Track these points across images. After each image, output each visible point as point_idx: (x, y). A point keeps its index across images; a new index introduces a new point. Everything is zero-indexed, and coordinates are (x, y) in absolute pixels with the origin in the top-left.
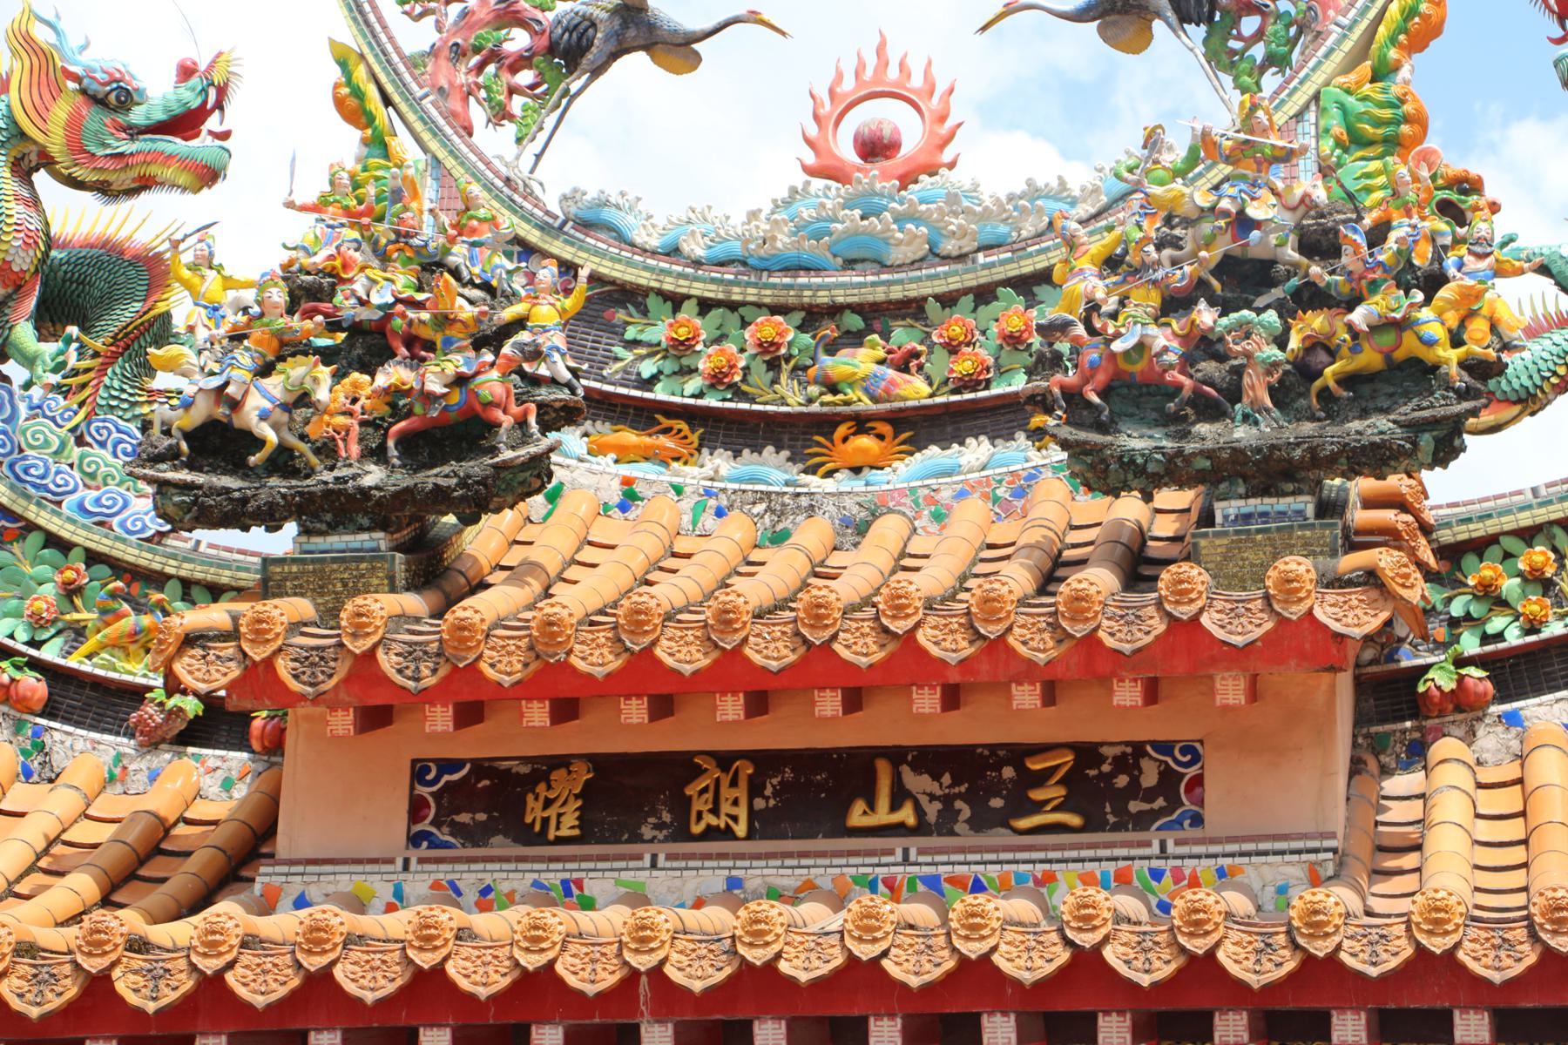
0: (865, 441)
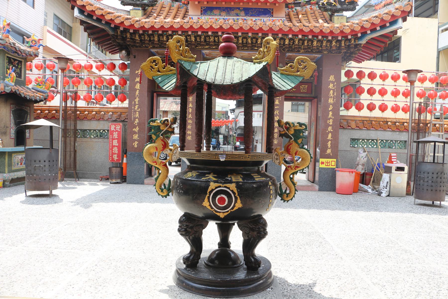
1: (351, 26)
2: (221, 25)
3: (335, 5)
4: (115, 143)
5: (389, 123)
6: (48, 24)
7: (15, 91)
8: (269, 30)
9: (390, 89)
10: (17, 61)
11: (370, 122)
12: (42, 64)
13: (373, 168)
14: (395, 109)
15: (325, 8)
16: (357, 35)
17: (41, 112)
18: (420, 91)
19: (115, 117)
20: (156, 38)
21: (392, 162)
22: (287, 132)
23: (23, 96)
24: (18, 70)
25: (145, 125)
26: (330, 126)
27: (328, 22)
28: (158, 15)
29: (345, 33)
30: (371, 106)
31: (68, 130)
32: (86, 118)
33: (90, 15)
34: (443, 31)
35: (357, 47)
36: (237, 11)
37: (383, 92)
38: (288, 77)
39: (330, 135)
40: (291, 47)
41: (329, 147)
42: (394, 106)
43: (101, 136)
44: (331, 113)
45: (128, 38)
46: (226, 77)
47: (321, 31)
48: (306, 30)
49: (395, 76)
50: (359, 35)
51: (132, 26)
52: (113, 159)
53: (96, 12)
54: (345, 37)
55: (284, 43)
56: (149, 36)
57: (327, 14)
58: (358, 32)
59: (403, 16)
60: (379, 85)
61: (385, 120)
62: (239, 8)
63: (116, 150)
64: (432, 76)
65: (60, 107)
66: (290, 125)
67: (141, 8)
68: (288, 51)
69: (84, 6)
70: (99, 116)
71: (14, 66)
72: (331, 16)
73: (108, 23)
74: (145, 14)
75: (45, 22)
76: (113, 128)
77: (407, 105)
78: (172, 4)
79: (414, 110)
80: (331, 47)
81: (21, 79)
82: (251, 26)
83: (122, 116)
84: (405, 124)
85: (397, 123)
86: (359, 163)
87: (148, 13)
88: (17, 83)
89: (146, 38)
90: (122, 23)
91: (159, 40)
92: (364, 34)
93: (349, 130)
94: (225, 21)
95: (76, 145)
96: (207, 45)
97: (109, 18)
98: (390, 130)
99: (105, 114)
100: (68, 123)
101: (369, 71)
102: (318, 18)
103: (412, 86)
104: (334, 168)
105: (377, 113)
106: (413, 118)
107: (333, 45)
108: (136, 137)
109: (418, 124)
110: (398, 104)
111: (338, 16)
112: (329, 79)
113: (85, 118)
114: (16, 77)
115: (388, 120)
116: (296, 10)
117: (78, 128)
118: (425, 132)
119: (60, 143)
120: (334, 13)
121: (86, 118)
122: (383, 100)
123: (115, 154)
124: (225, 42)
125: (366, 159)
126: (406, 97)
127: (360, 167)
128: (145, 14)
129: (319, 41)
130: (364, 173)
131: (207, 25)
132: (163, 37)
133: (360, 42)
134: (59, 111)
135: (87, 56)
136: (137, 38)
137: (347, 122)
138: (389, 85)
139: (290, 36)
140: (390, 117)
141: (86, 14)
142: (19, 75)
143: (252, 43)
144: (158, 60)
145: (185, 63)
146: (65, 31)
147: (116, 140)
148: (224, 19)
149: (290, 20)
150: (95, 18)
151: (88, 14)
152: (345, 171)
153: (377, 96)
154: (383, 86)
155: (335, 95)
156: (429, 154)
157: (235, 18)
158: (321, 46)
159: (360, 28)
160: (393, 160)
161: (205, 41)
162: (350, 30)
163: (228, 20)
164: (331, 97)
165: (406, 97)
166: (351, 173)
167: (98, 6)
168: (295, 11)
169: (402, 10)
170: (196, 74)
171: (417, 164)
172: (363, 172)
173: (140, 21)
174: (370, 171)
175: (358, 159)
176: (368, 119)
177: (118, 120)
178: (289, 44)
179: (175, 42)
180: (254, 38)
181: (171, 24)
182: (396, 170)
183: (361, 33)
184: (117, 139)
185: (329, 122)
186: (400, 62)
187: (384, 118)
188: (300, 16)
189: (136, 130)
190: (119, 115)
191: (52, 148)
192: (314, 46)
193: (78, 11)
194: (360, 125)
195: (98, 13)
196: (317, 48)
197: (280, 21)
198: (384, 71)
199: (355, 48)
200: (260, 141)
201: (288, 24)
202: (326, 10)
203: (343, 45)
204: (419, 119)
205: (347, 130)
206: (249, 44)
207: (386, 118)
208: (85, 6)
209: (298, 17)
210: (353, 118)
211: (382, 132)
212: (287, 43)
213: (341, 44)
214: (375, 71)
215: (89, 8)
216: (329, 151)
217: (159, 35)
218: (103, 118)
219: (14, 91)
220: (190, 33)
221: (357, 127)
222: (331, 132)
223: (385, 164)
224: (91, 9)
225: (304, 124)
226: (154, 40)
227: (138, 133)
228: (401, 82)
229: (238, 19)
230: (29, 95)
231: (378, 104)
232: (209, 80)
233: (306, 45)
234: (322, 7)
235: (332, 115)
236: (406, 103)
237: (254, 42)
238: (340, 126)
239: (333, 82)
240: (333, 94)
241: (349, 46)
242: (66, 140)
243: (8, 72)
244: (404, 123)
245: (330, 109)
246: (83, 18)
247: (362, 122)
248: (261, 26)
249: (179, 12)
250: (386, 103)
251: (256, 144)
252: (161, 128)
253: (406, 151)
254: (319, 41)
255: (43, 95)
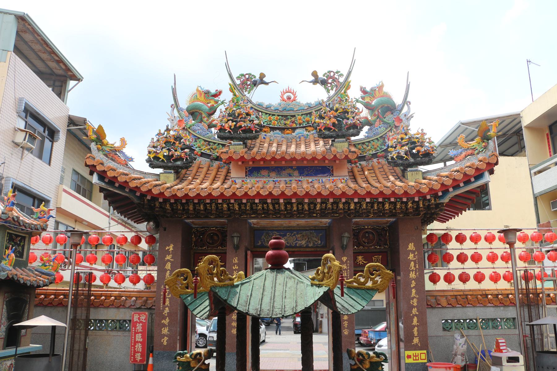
0: (288, 131)
1: (429, 183)
2: (270, 190)
3: (406, 158)
4: (139, 338)
5: (489, 296)
6: (65, 181)
7: (13, 277)
8: (329, 194)
9: (485, 254)
10: (19, 237)
11: (464, 297)
12: (51, 238)
13: (476, 358)
14: (495, 278)
15: (395, 162)
16: (437, 194)
17: (45, 297)
18: (523, 253)
19: (139, 303)
20: (191, 207)
21: (501, 351)
22: (361, 367)
23: (22, 282)
24: (20, 248)
25: (177, 316)
26: (414, 307)
27: (401, 178)
28: (194, 178)
29: (423, 193)
30: (464, 277)
31: (78, 320)
32: (103, 305)
33: (112, 181)
34: (535, 174)
35: (439, 207)
36: (289, 171)
37: (476, 258)
38: (357, 291)
39: (415, 320)
40: (358, 212)
41: (416, 335)
42: (493, 274)
43: (120, 328)
44: (414, 291)
45: (157, 208)
46: (275, 305)
47: (393, 192)
48: (375, 192)
49: (490, 236)
50: (440, 194)
51: (162, 194)
52: (135, 360)
53: (119, 179)
54: (423, 197)
55: (349, 208)
56: (182, 204)
57: (398, 170)
58: (439, 190)
59: (489, 168)
60: (471, 249)
61: (484, 293)
62: (291, 168)
63: (139, 347)
64: (534, 234)
65: (69, 290)
66: (364, 357)
67: (173, 171)
68: (354, 216)
69: (105, 172)
70: (119, 301)
71: (16, 244)
72: (404, 171)
73: (134, 190)
74: (177, 178)
75: (62, 178)
76: (136, 318)
77: (509, 272)
78: (211, 164)
79: (519, 279)
80: (407, 209)
81: (22, 260)
82: (307, 191)
83: (149, 302)
84: (510, 296)
85: (500, 296)
86: (456, 352)
87: (181, 176)
88: (17, 264)
89: (179, 207)
90: (150, 191)
91: (194, 209)
92: (446, 192)
93: (439, 309)
94: (275, 183)
95: (87, 341)
96: (254, 213)
97: (134, 185)
98: (492, 305)
99: (126, 299)
100: (79, 311)
101: (457, 233)
102: (389, 174)
103: (512, 249)
104: (425, 363)
105: (472, 285)
106: (520, 287)
107: (409, 207)
108: (165, 331)
109: (527, 294)
110: (498, 271)
111: (411, 171)
112: (408, 247)
113: (101, 305)
114: (16, 256)
115: (488, 292)
116: (360, 165)
117: (91, 318)
118: (538, 305)
119: (66, 339)
120: (408, 167)
121: (103, 305)
122: (478, 268)
123: (138, 352)
124: (273, 249)
125: (465, 347)
126: (507, 262)
127: (459, 357)
128: (177, 178)
129: (391, 203)
130: (465, 365)
131: (253, 191)
132: (200, 206)
133: (442, 201)
134: (68, 295)
135: (109, 217)
136: (168, 207)
137: (436, 299)
138: (483, 248)
139: (356, 200)
140: (489, 288)
141: (107, 180)
142: (20, 254)
143: (309, 209)
144: (188, 273)
145: (220, 289)
146: (83, 189)
147: (140, 334)
148: (274, 181)
149: (354, 179)
150: (117, 185)
151: (109, 180)
152: (440, 367)
153: (470, 263)
154: (476, 251)
155: (417, 267)
156: (548, 335)
157: (287, 179)
158: (395, 208)
159: (440, 185)
160: (501, 348)
161: (252, 208)
162: (428, 189)
163: (278, 183)
164: (413, 271)
165: (507, 262)
166: (448, 370)
167: (121, 171)
168: (360, 167)
169: (487, 162)
170: (235, 306)
171: (535, 355)
172: (464, 363)
173: (172, 187)
174: (473, 362)
175: (455, 347)
176: (462, 293)
177: (143, 307)
178: (355, 208)
179: (207, 264)
180: (312, 203)
181: (210, 192)
182: (508, 362)
183: (442, 192)
184: (141, 332)
185: (413, 303)
186: (490, 209)
187: (482, 290)
188: (366, 173)
189: (166, 321)
190: (144, 301)
191: (54, 355)
192: (386, 210)
193: (97, 178)
194: (453, 301)
195: (121, 179)
196: (390, 211)
197: (343, 181)
198: (474, 231)
199: (436, 209)
200: (325, 315)
201: (352, 185)
202: (397, 165)
203: (421, 206)
204: (527, 289)
205: (436, 309)
206: (306, 210)
207: (485, 290)
208: (106, 172)
209: (364, 174)
210: (442, 294)
211: (481, 308)
212: (352, 208)
213: (419, 204)
214: (464, 233)
215: (110, 174)
216: (416, 341)
217: (195, 204)
218: (124, 306)
219: (10, 276)
220: (232, 201)
221: (449, 304)
222: (416, 315)
223: (492, 354)
224: (112, 175)
225: (382, 354)
226: (188, 209)
227: (169, 326)
228: (497, 243)
229: (291, 181)
230: (30, 281)
231: (472, 273)
232: (252, 311)
233: (376, 208)
234: (392, 162)
235: (416, 293)
236: (508, 270)
237: (312, 208)
238: (427, 305)
239: (413, 252)
240: (415, 266)
241: (429, 205)
242: (74, 332)
243: (7, 252)
244: (508, 295)
245: (412, 286)
246: (103, 185)
247: (454, 297)
248: (319, 191)
249: (219, 173)
250: (482, 271)
251: (321, 319)
252: (192, 365)
253: (517, 332)
254: (391, 203)
255: (48, 279)
